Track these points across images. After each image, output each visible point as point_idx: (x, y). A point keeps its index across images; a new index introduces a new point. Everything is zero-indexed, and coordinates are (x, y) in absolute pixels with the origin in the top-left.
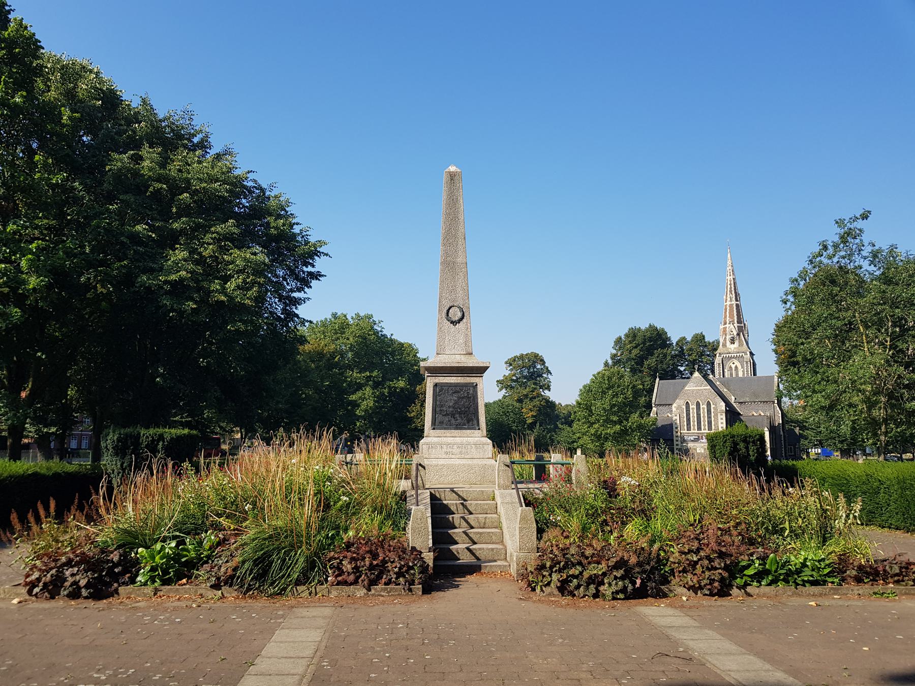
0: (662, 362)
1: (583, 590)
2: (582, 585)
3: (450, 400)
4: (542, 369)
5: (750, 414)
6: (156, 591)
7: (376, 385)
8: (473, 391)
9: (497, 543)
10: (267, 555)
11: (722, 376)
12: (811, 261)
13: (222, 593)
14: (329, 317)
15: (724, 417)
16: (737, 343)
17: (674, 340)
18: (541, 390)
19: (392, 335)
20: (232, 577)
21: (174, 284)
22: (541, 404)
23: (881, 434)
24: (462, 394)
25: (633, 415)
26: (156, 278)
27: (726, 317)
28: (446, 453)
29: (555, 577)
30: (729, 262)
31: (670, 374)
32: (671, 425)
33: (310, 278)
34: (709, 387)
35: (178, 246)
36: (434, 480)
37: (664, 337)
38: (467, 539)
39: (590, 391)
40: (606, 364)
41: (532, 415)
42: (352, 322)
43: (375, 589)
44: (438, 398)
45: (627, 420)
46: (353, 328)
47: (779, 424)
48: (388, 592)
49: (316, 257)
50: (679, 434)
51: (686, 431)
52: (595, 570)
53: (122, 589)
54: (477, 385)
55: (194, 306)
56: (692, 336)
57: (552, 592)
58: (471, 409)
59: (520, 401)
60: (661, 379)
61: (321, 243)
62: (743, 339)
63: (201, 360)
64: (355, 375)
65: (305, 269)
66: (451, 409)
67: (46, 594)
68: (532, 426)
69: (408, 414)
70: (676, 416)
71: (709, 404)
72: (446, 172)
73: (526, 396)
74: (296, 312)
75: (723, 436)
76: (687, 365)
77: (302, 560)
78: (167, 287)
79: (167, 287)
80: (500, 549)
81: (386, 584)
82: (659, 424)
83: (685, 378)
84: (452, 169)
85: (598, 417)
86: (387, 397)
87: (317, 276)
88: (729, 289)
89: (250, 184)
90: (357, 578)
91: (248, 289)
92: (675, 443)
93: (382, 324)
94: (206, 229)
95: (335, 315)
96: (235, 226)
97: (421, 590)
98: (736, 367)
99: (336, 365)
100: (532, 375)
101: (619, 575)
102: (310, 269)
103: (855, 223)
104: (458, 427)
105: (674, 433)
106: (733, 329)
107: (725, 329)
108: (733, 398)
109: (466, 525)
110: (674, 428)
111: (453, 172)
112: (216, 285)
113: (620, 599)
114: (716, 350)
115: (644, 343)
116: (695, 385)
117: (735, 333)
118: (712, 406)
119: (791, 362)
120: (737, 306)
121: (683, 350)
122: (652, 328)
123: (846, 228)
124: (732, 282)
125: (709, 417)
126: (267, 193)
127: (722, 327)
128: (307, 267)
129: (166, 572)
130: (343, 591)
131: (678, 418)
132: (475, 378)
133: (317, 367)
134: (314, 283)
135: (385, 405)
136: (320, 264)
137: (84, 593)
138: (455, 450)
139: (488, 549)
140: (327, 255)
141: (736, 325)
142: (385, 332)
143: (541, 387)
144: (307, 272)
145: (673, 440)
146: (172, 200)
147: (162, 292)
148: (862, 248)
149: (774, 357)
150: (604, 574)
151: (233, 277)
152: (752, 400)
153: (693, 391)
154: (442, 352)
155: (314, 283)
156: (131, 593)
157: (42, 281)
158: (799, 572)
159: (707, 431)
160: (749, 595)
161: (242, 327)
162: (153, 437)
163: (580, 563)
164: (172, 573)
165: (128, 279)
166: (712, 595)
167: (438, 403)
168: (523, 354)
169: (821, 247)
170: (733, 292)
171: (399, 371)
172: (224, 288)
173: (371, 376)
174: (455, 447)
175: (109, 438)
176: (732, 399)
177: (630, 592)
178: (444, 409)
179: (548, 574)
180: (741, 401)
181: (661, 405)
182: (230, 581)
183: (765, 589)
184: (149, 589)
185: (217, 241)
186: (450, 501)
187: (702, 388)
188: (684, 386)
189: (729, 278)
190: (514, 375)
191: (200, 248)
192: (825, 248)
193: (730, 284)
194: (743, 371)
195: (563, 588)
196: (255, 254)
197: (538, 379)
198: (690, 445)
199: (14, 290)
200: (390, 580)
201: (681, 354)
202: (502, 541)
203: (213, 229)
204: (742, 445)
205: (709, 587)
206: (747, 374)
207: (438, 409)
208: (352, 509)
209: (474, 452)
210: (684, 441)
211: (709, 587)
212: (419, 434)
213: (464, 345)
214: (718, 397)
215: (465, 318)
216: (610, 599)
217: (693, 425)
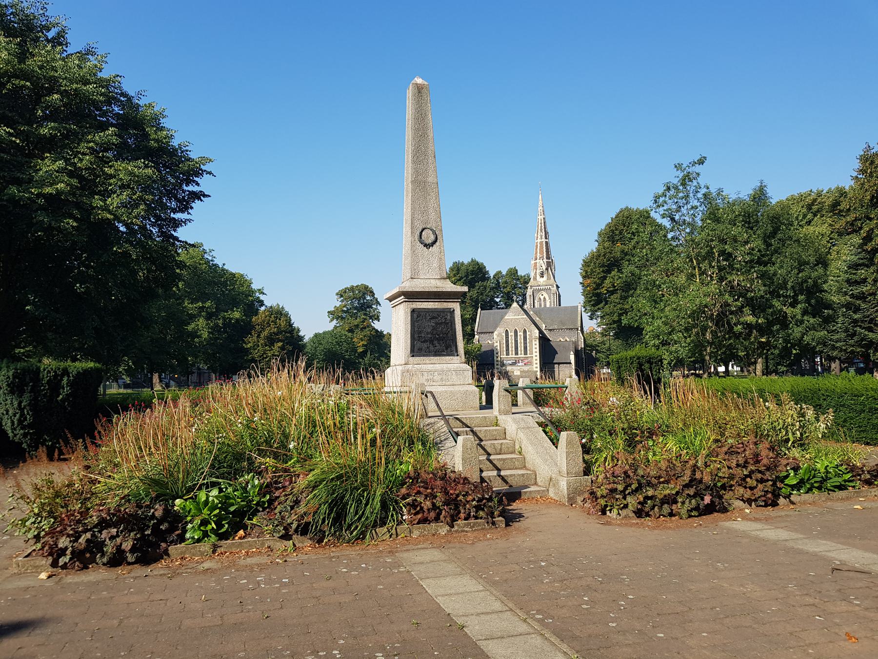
0: (482, 294)
1: (658, 510)
2: (657, 505)
3: (428, 326)
4: (371, 300)
5: (558, 340)
6: (215, 547)
7: (209, 317)
8: (451, 317)
9: (519, 469)
11: (532, 307)
12: (656, 202)
13: (293, 543)
15: (537, 342)
16: (545, 276)
17: (492, 274)
18: (371, 320)
19: (224, 264)
21: (48, 197)
22: (371, 334)
23: (706, 354)
24: (439, 320)
26: (26, 190)
27: (536, 253)
30: (540, 203)
31: (489, 305)
32: (492, 351)
35: (48, 155)
41: (363, 345)
43: (458, 525)
47: (582, 348)
48: (471, 527)
51: (505, 356)
53: (172, 549)
54: (454, 310)
55: (75, 224)
56: (507, 270)
57: (628, 515)
58: (449, 335)
59: (351, 331)
62: (551, 273)
63: (78, 285)
66: (429, 336)
67: (77, 563)
68: (363, 354)
69: (244, 345)
70: (497, 342)
71: (525, 331)
72: (413, 84)
73: (357, 326)
74: (175, 234)
75: (630, 358)
76: (502, 297)
78: (41, 201)
79: (41, 201)
80: (530, 474)
81: (466, 519)
82: (483, 349)
83: (500, 308)
84: (419, 81)
87: (198, 196)
88: (539, 228)
90: (439, 514)
96: (116, 135)
97: (504, 522)
98: (545, 298)
101: (692, 494)
103: (694, 167)
104: (437, 354)
106: (542, 264)
107: (536, 264)
108: (544, 326)
109: (483, 452)
110: (495, 353)
111: (420, 84)
112: (97, 201)
113: (695, 516)
115: (467, 276)
116: (514, 315)
117: (544, 268)
119: (596, 294)
120: (547, 243)
121: (499, 283)
122: (474, 263)
123: (685, 171)
125: (525, 343)
127: (533, 262)
130: (425, 530)
132: (453, 303)
136: (204, 184)
137: (130, 558)
138: (437, 377)
139: (519, 475)
140: (210, 173)
141: (545, 260)
142: (216, 261)
143: (371, 317)
144: (188, 191)
145: (494, 364)
146: (38, 102)
148: (699, 190)
149: (580, 289)
150: (677, 493)
151: (115, 192)
152: (559, 328)
154: (416, 277)
155: (197, 204)
156: (184, 553)
158: (824, 480)
160: (793, 503)
162: (55, 372)
164: (226, 526)
166: (766, 506)
170: (543, 231)
171: (234, 302)
173: (203, 307)
174: (436, 373)
176: (543, 327)
177: (703, 509)
178: (423, 335)
179: (621, 497)
180: (551, 328)
181: (482, 333)
183: (808, 497)
184: (206, 546)
188: (502, 317)
189: (540, 217)
191: (74, 158)
193: (541, 223)
194: (550, 302)
197: (368, 309)
198: (509, 368)
200: (469, 514)
202: (525, 467)
205: (763, 498)
206: (554, 304)
207: (416, 336)
209: (454, 379)
210: (503, 365)
211: (763, 498)
213: (438, 269)
214: (533, 325)
215: (438, 241)
216: (687, 517)
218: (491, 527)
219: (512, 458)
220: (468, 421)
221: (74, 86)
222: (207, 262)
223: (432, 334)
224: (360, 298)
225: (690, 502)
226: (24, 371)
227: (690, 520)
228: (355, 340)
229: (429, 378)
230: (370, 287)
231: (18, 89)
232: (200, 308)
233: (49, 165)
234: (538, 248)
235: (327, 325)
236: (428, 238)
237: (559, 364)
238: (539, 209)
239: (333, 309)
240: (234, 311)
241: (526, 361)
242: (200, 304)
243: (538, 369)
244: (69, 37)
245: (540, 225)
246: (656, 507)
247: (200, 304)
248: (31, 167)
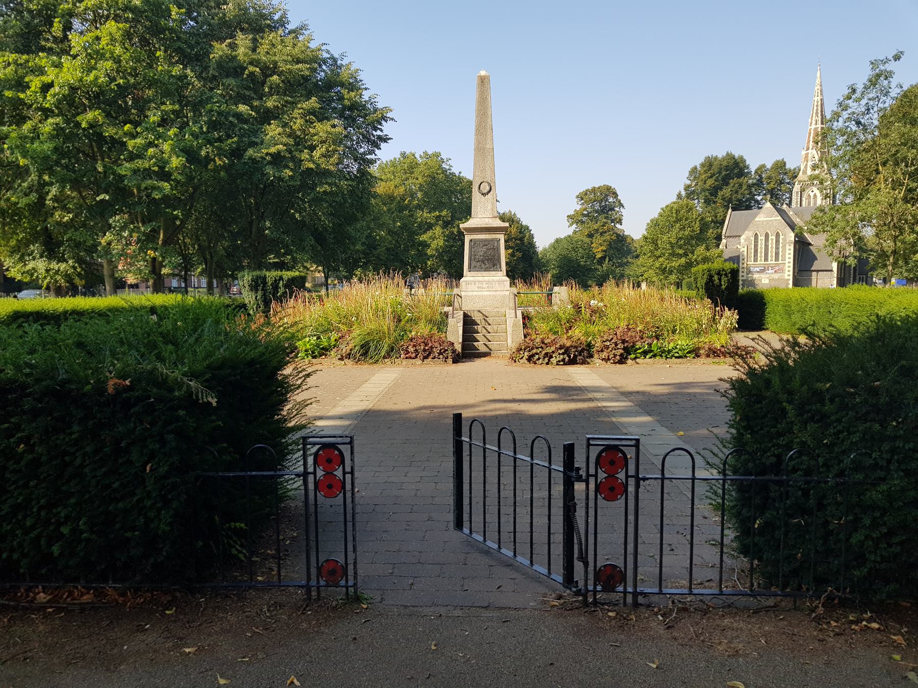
0: (737, 192)
3: (481, 251)
7: (446, 224)
10: (367, 343)
14: (398, 156)
17: (753, 168)
19: (460, 173)
20: (349, 354)
27: (809, 142)
28: (478, 287)
29: (526, 354)
30: (818, 81)
31: (741, 205)
32: (738, 257)
34: (780, 218)
36: (468, 306)
37: (741, 165)
38: (485, 340)
39: (657, 224)
40: (679, 196)
45: (693, 253)
46: (422, 168)
49: (383, 122)
50: (745, 265)
52: (549, 350)
55: (291, 174)
56: (773, 162)
59: (590, 236)
60: (734, 209)
64: (424, 215)
71: (778, 235)
77: (386, 346)
78: (268, 158)
84: (483, 73)
85: (663, 251)
87: (385, 139)
88: (815, 111)
89: (326, 55)
90: (417, 355)
91: (330, 157)
92: (741, 274)
94: (294, 104)
95: (403, 155)
98: (815, 195)
99: (407, 207)
102: (379, 133)
104: (486, 270)
105: (741, 264)
107: (807, 155)
112: (305, 155)
114: (796, 177)
115: (720, 173)
118: (781, 237)
122: (730, 157)
124: (819, 104)
125: (777, 248)
126: (339, 62)
127: (804, 152)
128: (376, 131)
129: (313, 352)
131: (745, 249)
133: (389, 210)
134: (383, 145)
135: (455, 244)
136: (387, 128)
138: (485, 285)
143: (612, 221)
146: (264, 83)
147: (265, 162)
150: (553, 352)
153: (763, 222)
155: (383, 145)
157: (181, 161)
159: (763, 262)
160: (638, 363)
161: (328, 188)
163: (542, 347)
165: (237, 153)
168: (595, 188)
169: (850, 91)
170: (819, 115)
172: (311, 156)
173: (439, 216)
175: (245, 279)
182: (348, 356)
185: (303, 116)
186: (477, 317)
187: (773, 218)
189: (816, 99)
190: (585, 210)
192: (854, 91)
193: (817, 106)
195: (529, 359)
196: (334, 126)
197: (610, 213)
198: (756, 276)
199: (162, 168)
201: (759, 183)
203: (299, 106)
204: (716, 277)
208: (414, 321)
210: (749, 272)
212: (460, 275)
214: (788, 228)
217: (760, 257)
221: (288, 67)
222: (444, 171)
226: (258, 277)
231: (252, 74)
233: (273, 130)
234: (812, 135)
235: (566, 230)
237: (818, 271)
238: (816, 88)
241: (777, 268)
242: (437, 213)
243: (791, 278)
244: (290, 16)
245: (815, 108)
247: (437, 213)
248: (262, 132)
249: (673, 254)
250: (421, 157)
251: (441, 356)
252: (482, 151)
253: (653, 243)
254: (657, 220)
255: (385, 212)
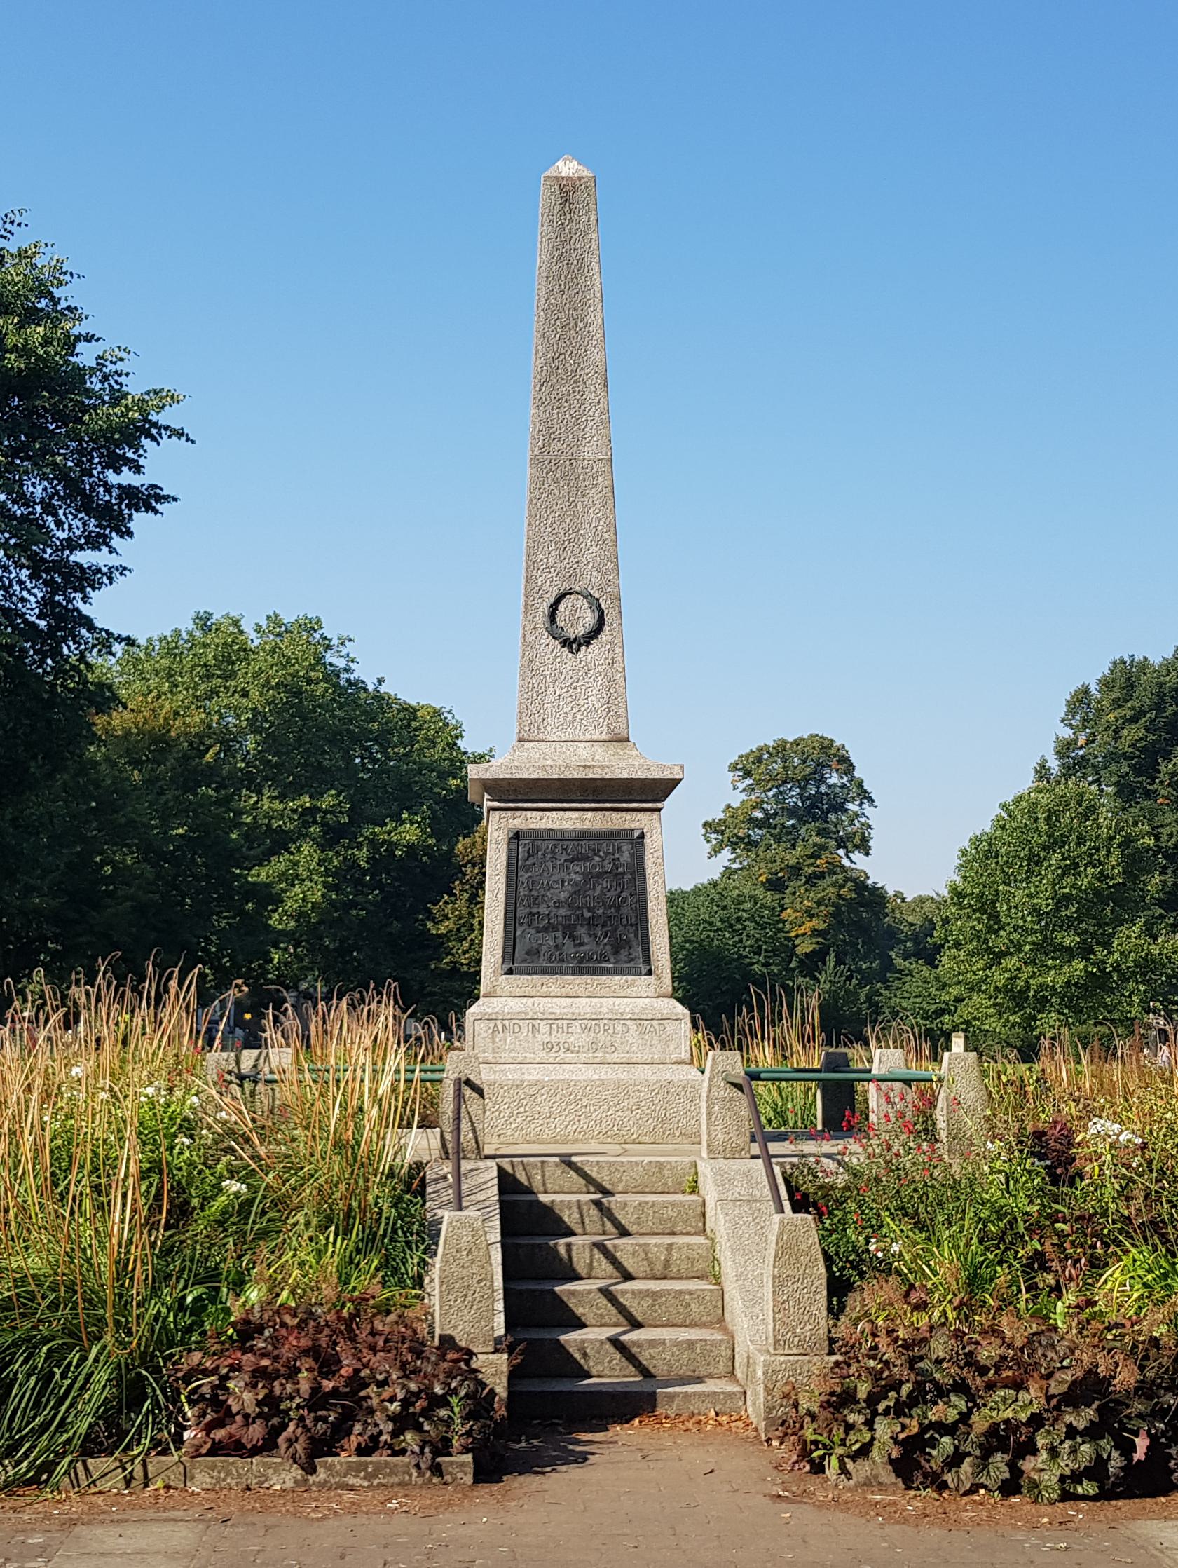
1: (970, 1470)
2: (969, 1454)
4: (843, 786)
7: (332, 837)
8: (632, 855)
9: (703, 1325)
18: (841, 852)
19: (380, 681)
22: (840, 896)
24: (597, 864)
25: (1123, 930)
28: (549, 1047)
29: (884, 1429)
33: (1109, 1478)
40: (1042, 771)
42: (256, 643)
43: (330, 1468)
44: (524, 876)
45: (1107, 945)
46: (261, 662)
54: (642, 836)
57: (876, 1477)
58: (624, 911)
59: (775, 885)
61: (163, 398)
65: (111, 477)
69: (430, 925)
72: (547, 178)
73: (795, 870)
74: (85, 609)
80: (714, 1344)
81: (362, 1451)
84: (568, 167)
85: (1016, 936)
86: (365, 872)
87: (148, 499)
90: (275, 1432)
93: (349, 648)
95: (203, 621)
97: (470, 1469)
99: (209, 774)
100: (813, 806)
101: (1081, 1424)
102: (127, 477)
104: (585, 966)
111: (568, 178)
113: (1084, 1498)
115: (1159, 707)
128: (118, 471)
130: (228, 1474)
132: (639, 815)
133: (149, 782)
135: (360, 898)
138: (577, 1037)
139: (677, 1343)
140: (179, 434)
142: (359, 673)
143: (841, 843)
150: (1036, 1421)
154: (535, 735)
155: (140, 521)
167: (523, 892)
168: (786, 742)
173: (314, 810)
177: (1117, 1477)
178: (543, 909)
190: (758, 805)
197: (832, 817)
202: (722, 1320)
207: (522, 911)
215: (606, 628)
218: (430, 1480)
219: (681, 1292)
220: (606, 1172)
222: (332, 675)
223: (570, 906)
224: (806, 780)
225: (1074, 1451)
227: (1070, 1509)
228: (788, 914)
229: (553, 1039)
230: (837, 743)
232: (306, 811)
236: (575, 620)
239: (722, 816)
240: (403, 823)
242: (306, 801)
246: (968, 1460)
247: (306, 801)
249: (1046, 947)
250: (258, 630)
251: (409, 1437)
252: (564, 465)
253: (982, 910)
254: (991, 841)
255: (136, 788)
